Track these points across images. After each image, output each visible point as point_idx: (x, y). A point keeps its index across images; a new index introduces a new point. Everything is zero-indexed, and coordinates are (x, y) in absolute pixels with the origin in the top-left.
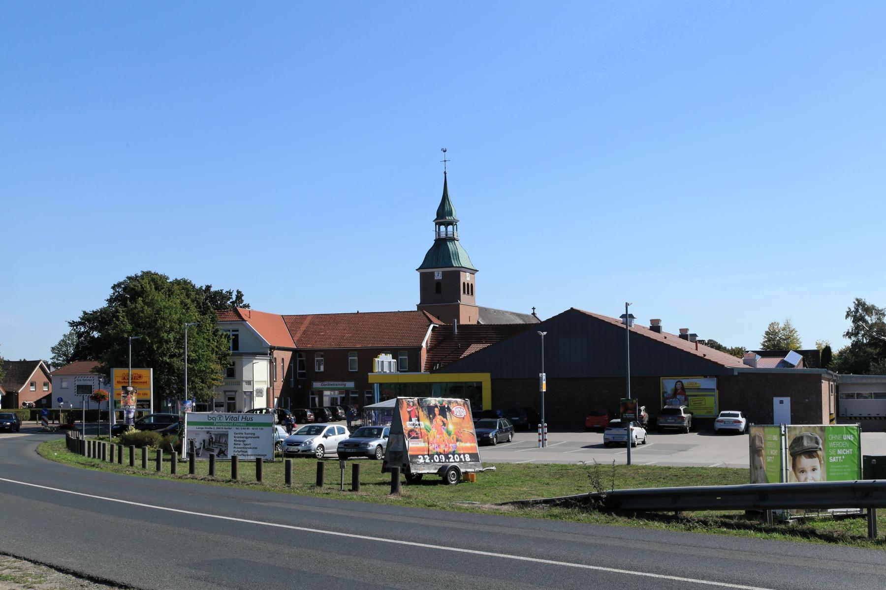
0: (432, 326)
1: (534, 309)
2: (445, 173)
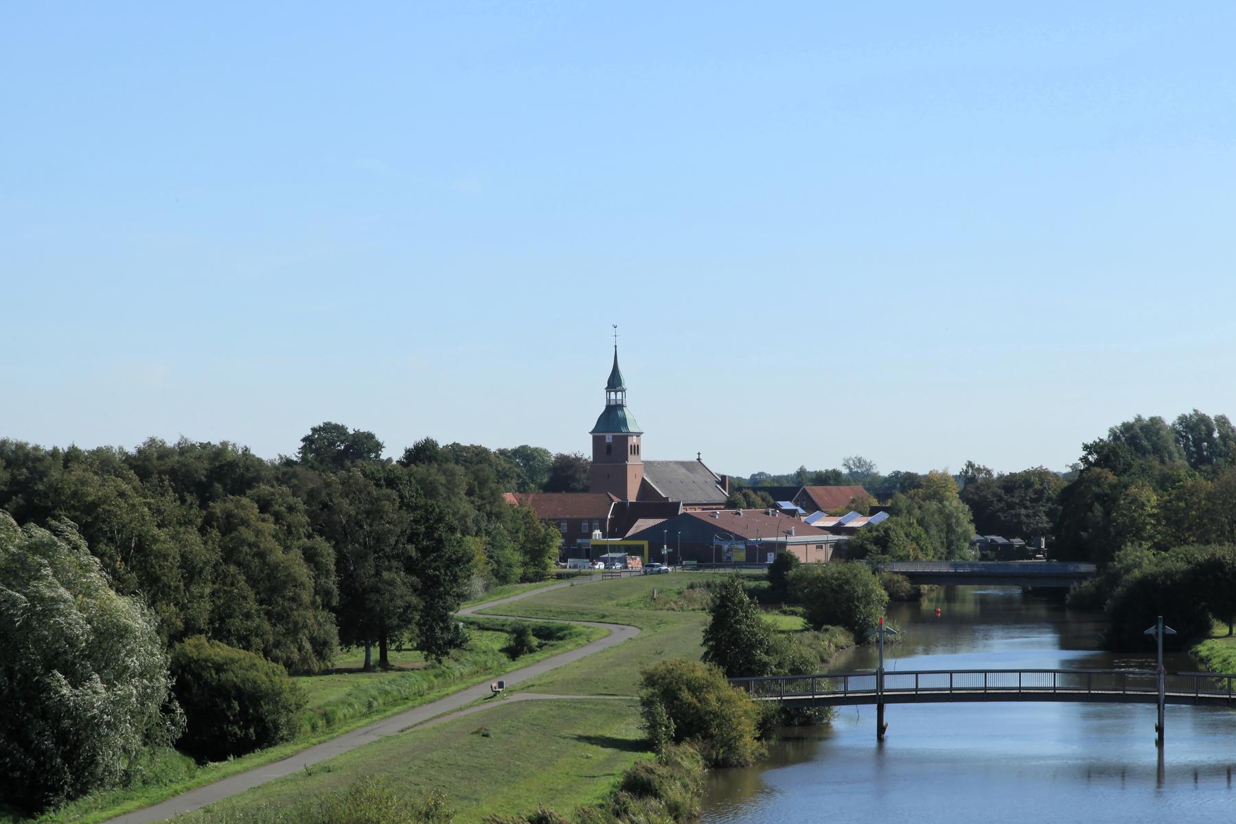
0: (613, 504)
1: (699, 454)
2: (616, 346)
